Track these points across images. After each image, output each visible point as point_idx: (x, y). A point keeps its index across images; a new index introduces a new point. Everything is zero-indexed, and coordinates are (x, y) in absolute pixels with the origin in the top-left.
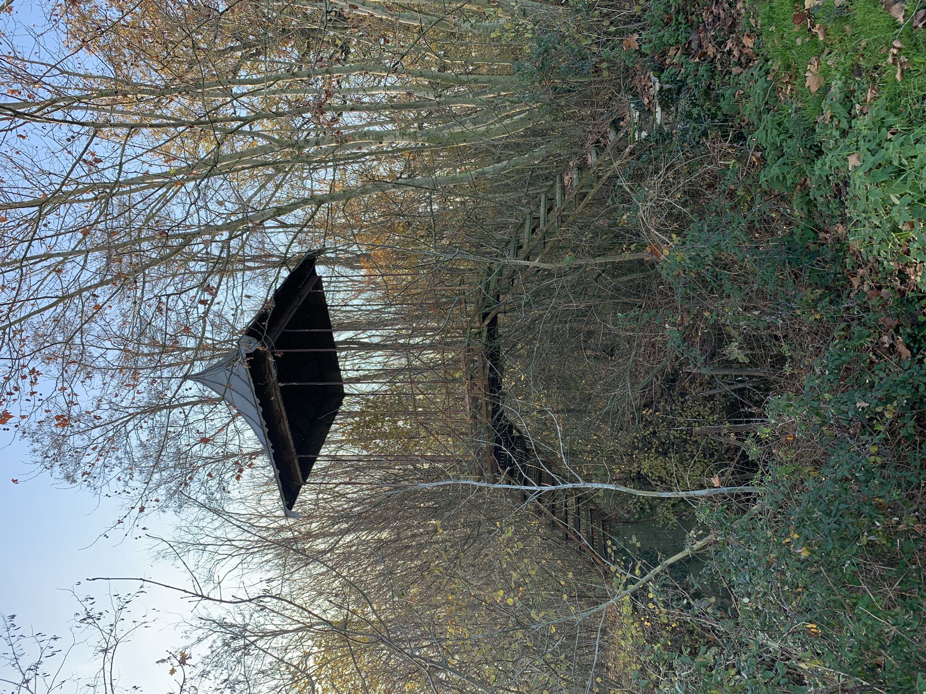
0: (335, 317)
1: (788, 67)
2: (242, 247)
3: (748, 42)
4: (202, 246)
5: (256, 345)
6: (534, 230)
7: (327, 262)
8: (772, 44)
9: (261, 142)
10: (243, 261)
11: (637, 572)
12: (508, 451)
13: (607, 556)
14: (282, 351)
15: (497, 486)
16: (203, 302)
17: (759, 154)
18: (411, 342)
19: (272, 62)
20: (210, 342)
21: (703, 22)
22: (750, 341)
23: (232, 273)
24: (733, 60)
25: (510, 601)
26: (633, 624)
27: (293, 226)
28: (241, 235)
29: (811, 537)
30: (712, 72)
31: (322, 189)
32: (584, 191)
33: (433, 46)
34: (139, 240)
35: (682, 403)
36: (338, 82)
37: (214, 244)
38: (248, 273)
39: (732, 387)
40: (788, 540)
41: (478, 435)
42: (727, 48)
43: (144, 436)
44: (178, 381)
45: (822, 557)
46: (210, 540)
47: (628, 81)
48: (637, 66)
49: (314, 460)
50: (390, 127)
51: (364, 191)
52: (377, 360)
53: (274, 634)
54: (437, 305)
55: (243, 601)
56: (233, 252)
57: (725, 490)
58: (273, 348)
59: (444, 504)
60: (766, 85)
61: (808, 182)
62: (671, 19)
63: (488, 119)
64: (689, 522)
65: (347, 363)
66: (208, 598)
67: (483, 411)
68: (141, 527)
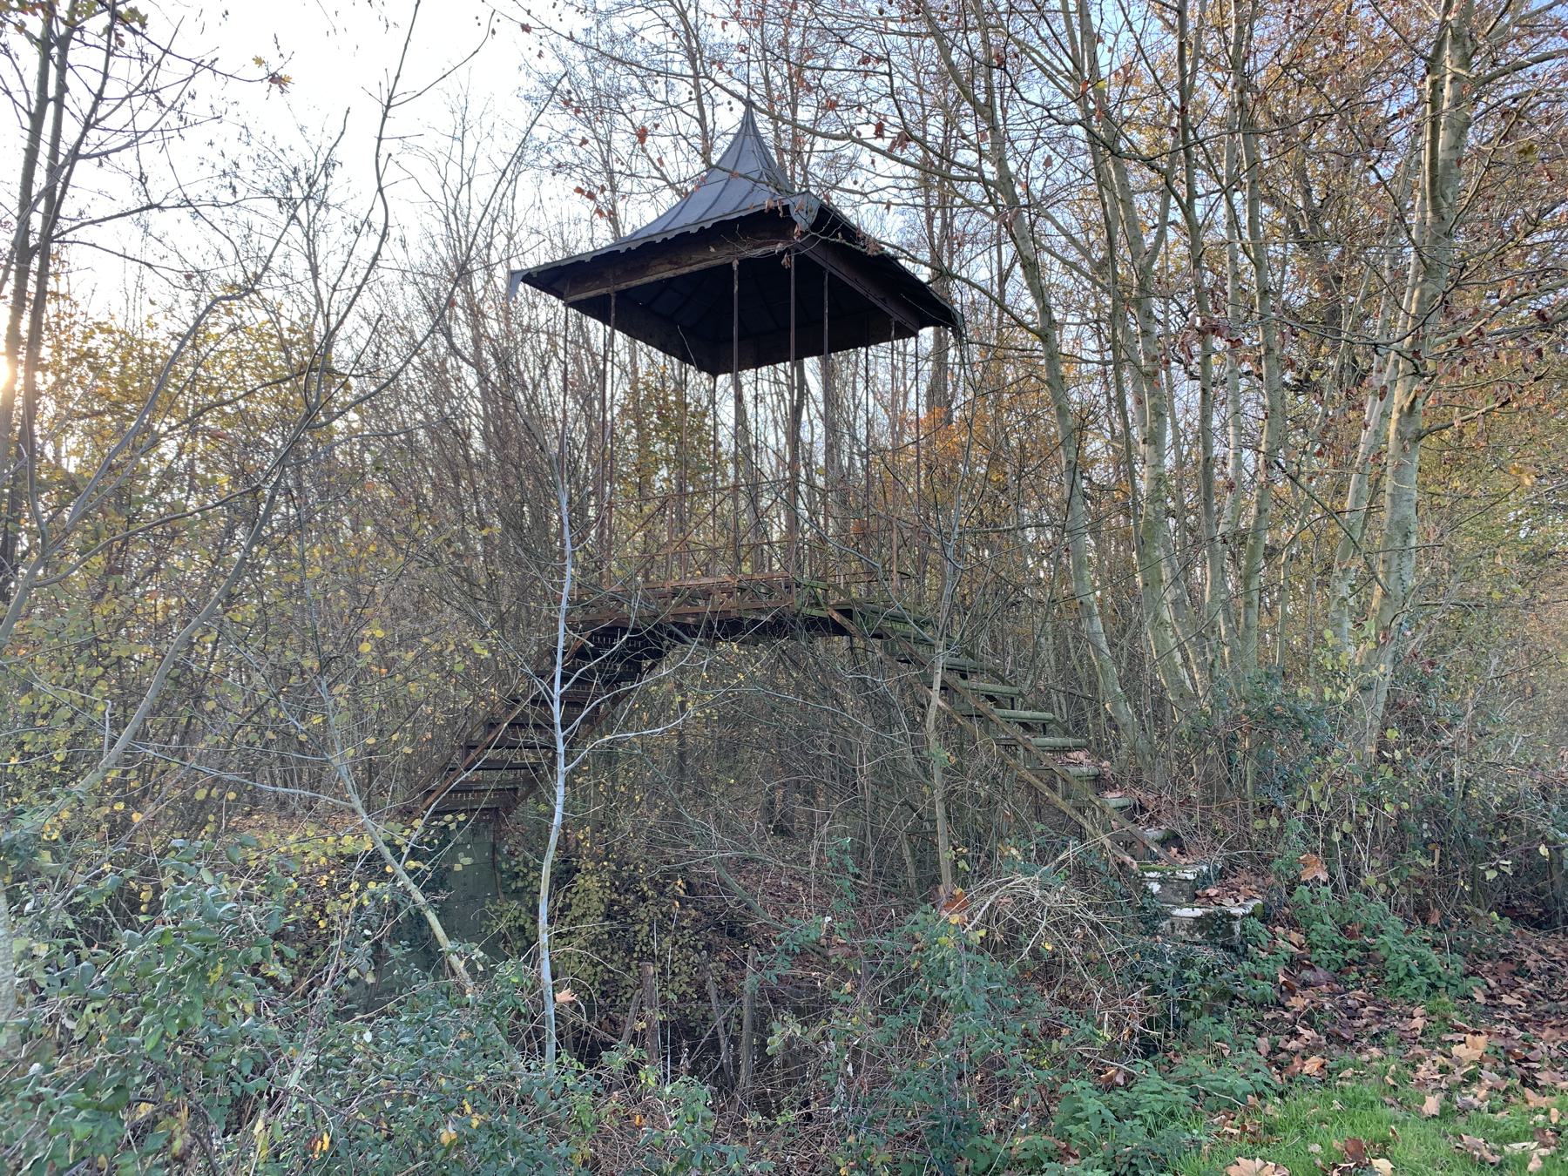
1: (1270, 1130)
3: (1312, 1065)
5: (802, 222)
6: (991, 698)
8: (1308, 1104)
9: (1149, 240)
11: (412, 864)
12: (619, 650)
13: (438, 813)
17: (1120, 1079)
19: (1285, 262)
21: (1348, 991)
22: (796, 1054)
24: (1281, 1040)
25: (366, 648)
26: (325, 854)
27: (1002, 292)
29: (475, 1147)
30: (1260, 1005)
31: (1066, 339)
32: (1060, 783)
33: (1307, 534)
34: (984, 28)
35: (694, 947)
36: (1248, 373)
39: (721, 1030)
40: (468, 1109)
41: (645, 598)
42: (1301, 1031)
45: (439, 1165)
46: (469, 152)
47: (1245, 861)
48: (1272, 879)
49: (606, 321)
50: (1169, 462)
51: (1062, 412)
52: (774, 438)
53: (311, 256)
55: (379, 179)
57: (550, 1011)
59: (529, 544)
60: (1239, 1093)
61: (1072, 1161)
62: (1351, 936)
63: (1182, 625)
64: (496, 948)
65: (766, 384)
66: (385, 116)
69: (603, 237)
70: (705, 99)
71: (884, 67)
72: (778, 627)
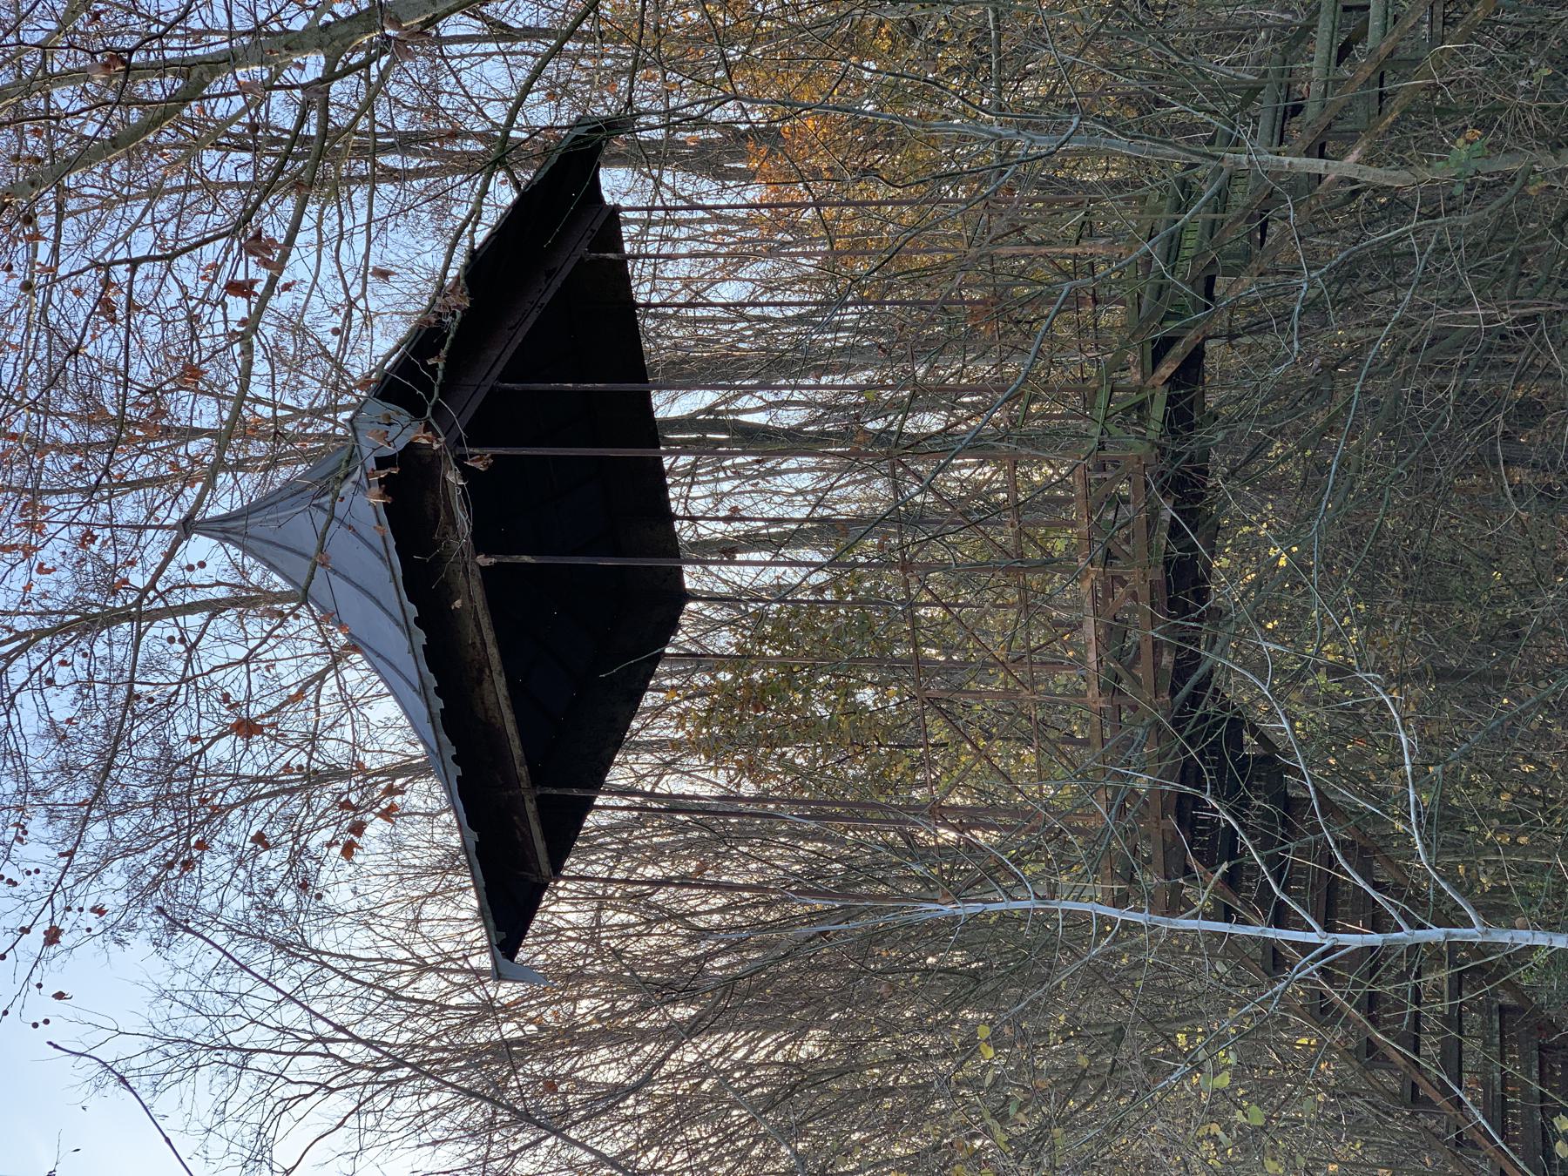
0: (661, 339)
2: (368, 106)
4: (238, 102)
5: (406, 432)
7: (645, 157)
10: (370, 150)
12: (1224, 802)
14: (489, 452)
15: (1183, 923)
16: (240, 288)
18: (909, 427)
20: (266, 412)
23: (336, 190)
27: (530, 33)
28: (365, 65)
37: (278, 97)
38: (385, 189)
43: (62, 706)
44: (166, 537)
49: (587, 806)
52: (792, 489)
54: (999, 306)
56: (339, 118)
58: (459, 442)
65: (696, 491)
67: (1143, 671)
68: (50, 989)
69: (425, 795)
70: (175, 600)
71: (120, 273)
72: (1186, 485)
